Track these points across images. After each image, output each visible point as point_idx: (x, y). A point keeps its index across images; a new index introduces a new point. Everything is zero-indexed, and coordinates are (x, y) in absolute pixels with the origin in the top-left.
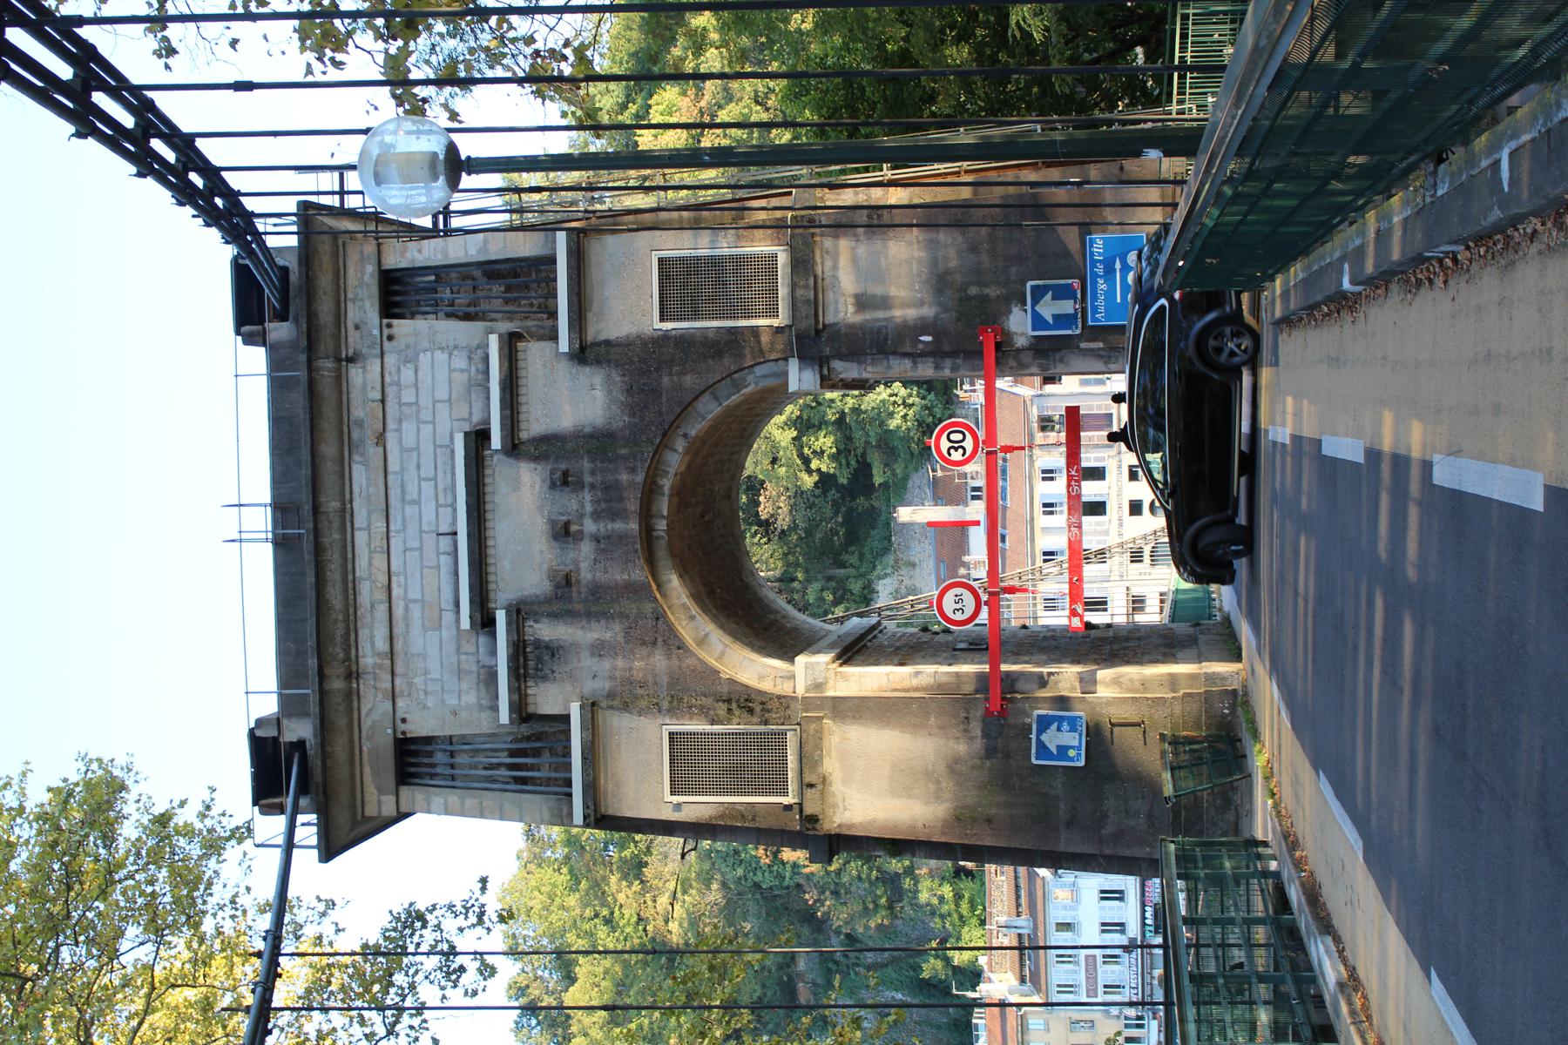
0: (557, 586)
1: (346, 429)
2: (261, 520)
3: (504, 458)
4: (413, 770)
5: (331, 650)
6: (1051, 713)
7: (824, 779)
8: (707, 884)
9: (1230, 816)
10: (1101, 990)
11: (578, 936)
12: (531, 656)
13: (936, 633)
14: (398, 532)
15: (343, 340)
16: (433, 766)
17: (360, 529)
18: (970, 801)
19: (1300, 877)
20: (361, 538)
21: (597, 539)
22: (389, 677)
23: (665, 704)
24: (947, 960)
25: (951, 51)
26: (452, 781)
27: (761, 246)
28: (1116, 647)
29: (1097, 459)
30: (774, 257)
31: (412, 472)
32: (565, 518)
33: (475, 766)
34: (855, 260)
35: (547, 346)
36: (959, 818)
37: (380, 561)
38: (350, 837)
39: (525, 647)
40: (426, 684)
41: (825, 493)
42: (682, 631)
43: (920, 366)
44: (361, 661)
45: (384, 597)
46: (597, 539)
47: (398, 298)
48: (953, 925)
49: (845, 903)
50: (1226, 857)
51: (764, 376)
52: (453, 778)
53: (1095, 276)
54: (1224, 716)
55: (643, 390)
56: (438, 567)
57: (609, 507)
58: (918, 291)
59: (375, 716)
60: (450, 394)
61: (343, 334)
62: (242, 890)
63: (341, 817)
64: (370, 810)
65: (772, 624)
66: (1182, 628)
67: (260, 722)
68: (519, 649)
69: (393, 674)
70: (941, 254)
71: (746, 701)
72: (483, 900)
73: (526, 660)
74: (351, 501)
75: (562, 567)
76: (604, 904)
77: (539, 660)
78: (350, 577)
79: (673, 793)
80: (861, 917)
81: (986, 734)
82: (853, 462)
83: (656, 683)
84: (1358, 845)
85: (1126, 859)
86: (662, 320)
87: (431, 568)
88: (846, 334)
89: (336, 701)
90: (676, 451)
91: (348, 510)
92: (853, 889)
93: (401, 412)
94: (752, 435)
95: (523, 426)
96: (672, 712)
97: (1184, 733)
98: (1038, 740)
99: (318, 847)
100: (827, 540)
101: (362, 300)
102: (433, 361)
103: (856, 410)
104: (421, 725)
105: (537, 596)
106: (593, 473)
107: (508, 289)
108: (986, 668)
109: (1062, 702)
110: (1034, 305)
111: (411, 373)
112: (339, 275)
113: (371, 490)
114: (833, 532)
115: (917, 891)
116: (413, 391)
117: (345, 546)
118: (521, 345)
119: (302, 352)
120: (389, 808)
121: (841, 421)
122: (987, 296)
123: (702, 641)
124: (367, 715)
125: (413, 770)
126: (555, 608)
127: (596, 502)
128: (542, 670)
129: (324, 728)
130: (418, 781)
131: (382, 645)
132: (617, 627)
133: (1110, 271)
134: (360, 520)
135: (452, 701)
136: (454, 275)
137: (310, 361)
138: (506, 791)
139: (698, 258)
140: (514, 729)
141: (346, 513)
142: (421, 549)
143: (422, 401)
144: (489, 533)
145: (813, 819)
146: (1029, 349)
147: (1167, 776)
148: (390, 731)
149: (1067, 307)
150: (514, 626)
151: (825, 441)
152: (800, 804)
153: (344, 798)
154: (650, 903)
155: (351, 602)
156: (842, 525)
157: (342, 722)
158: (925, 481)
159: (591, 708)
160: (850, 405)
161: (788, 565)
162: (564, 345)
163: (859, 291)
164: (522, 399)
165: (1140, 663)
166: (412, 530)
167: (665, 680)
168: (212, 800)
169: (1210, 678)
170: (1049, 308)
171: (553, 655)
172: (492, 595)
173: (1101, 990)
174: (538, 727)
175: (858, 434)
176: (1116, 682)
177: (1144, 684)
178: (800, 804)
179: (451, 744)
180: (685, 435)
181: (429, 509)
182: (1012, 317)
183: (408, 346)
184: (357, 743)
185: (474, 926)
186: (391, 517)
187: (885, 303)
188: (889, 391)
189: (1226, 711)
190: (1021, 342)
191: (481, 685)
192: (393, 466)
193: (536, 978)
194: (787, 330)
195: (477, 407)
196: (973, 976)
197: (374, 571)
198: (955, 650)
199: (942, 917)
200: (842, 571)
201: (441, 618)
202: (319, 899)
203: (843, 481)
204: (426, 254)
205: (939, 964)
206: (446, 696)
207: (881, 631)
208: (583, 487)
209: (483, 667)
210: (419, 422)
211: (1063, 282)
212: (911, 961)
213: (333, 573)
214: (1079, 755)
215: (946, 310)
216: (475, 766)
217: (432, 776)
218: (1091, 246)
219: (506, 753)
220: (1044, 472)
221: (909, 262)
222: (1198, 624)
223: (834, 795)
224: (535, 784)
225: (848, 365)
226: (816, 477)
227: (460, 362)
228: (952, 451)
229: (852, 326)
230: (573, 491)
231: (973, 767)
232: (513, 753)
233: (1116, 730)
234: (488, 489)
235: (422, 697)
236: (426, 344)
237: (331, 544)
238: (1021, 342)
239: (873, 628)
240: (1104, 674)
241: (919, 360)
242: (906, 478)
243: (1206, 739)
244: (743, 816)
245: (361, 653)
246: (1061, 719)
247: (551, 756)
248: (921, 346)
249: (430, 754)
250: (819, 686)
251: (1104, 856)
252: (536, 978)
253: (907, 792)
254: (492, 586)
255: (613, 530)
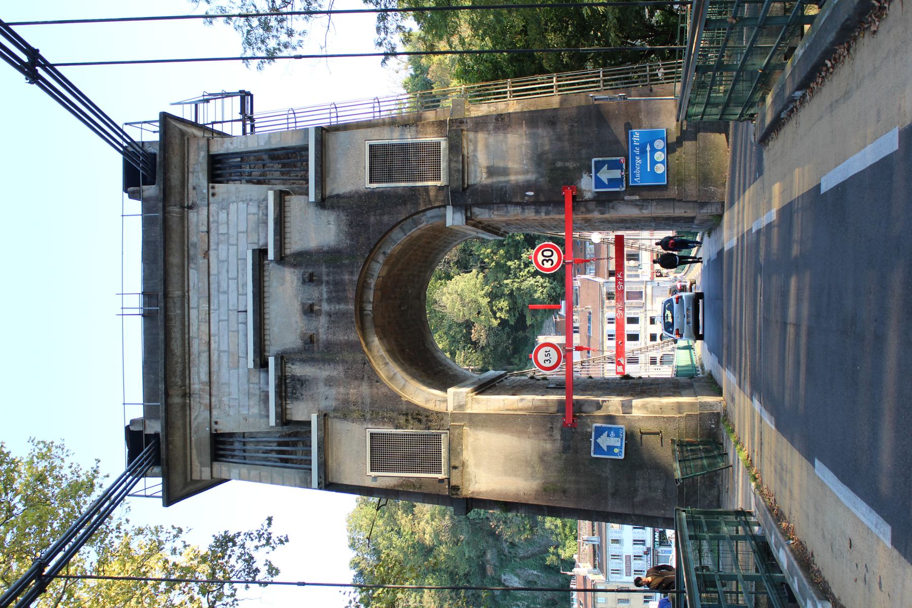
0: (305, 343)
1: (186, 248)
2: (136, 302)
3: (276, 265)
4: (222, 452)
5: (173, 379)
6: (604, 425)
7: (463, 464)
8: (444, 516)
9: (715, 492)
10: (633, 572)
11: (384, 539)
12: (289, 385)
13: (539, 380)
14: (215, 310)
15: (186, 196)
16: (233, 450)
17: (193, 308)
18: (552, 479)
19: (788, 544)
20: (193, 313)
21: (329, 315)
22: (208, 397)
23: (368, 416)
24: (558, 556)
25: (551, 36)
26: (244, 460)
27: (430, 138)
28: (645, 388)
29: (635, 313)
30: (439, 144)
31: (224, 273)
32: (310, 302)
33: (257, 451)
34: (487, 146)
35: (302, 198)
36: (546, 490)
37: (204, 327)
38: (184, 492)
39: (286, 380)
40: (229, 401)
41: (503, 329)
42: (380, 372)
43: (526, 211)
44: (192, 387)
45: (206, 348)
46: (329, 315)
47: (219, 172)
48: (562, 539)
49: (510, 527)
50: (723, 524)
51: (431, 217)
52: (245, 458)
53: (634, 155)
54: (711, 429)
55: (358, 225)
56: (238, 331)
57: (337, 296)
58: (525, 164)
59: (199, 420)
60: (247, 228)
61: (186, 192)
62: (124, 521)
63: (177, 479)
64: (196, 476)
65: (440, 372)
66: (683, 380)
67: (133, 422)
68: (282, 381)
69: (210, 395)
70: (540, 141)
71: (419, 415)
72: (270, 530)
73: (286, 388)
74: (188, 291)
75: (309, 332)
76: (396, 524)
77: (294, 388)
78: (187, 336)
79: (372, 470)
80: (518, 534)
81: (563, 438)
82: (517, 314)
83: (363, 403)
84: (884, 532)
85: (648, 517)
86: (371, 182)
87: (233, 332)
88: (481, 191)
89: (176, 412)
90: (378, 262)
91: (186, 297)
92: (514, 521)
93: (218, 239)
94: (432, 262)
95: (287, 246)
96: (372, 420)
97: (687, 439)
98: (595, 442)
99: (162, 497)
100: (504, 351)
101: (198, 172)
102: (237, 208)
103: (519, 289)
104: (226, 426)
105: (294, 349)
106: (328, 275)
107: (284, 166)
108: (564, 397)
109: (610, 419)
110: (596, 173)
111: (225, 215)
112: (184, 158)
113: (200, 285)
114: (507, 348)
115: (544, 522)
116: (226, 226)
117: (184, 318)
118: (287, 198)
119: (160, 201)
120: (206, 475)
121: (511, 294)
122: (567, 168)
123: (392, 378)
124: (195, 419)
125: (222, 452)
126: (304, 356)
127: (329, 292)
128: (295, 393)
129: (168, 425)
130: (224, 459)
131: (204, 377)
132: (341, 368)
133: (643, 152)
134: (193, 303)
135: (244, 412)
136: (252, 158)
137: (164, 207)
138: (276, 466)
139: (393, 145)
140: (280, 429)
141: (185, 298)
142: (228, 320)
143: (231, 232)
144: (266, 311)
145: (456, 488)
146: (593, 200)
147: (676, 465)
148: (208, 429)
149: (617, 174)
150: (279, 366)
151: (504, 304)
152: (449, 479)
153: (179, 468)
154: (416, 525)
155: (187, 351)
156: (511, 344)
157: (179, 423)
158: (551, 324)
159: (324, 417)
160: (516, 286)
161: (485, 363)
162: (312, 197)
163: (490, 164)
164: (287, 230)
165: (659, 396)
166: (223, 309)
167: (368, 401)
168: (98, 467)
169: (703, 405)
170: (605, 175)
171: (302, 385)
172: (267, 348)
173: (633, 572)
174: (294, 429)
175: (520, 301)
176: (644, 407)
177: (662, 408)
178: (449, 479)
179: (244, 437)
180: (384, 253)
181: (233, 296)
182: (582, 180)
183: (223, 200)
184: (188, 436)
185: (264, 545)
186: (211, 301)
187: (505, 172)
188: (535, 280)
189: (713, 426)
190: (588, 196)
191: (261, 402)
192: (213, 271)
193: (363, 559)
194: (445, 188)
195: (262, 236)
196: (571, 564)
197: (201, 333)
198: (547, 388)
199: (557, 535)
200: (511, 367)
201: (239, 362)
202: (173, 528)
203: (512, 323)
204: (235, 145)
205: (554, 558)
206: (241, 409)
207: (506, 378)
208: (322, 283)
209: (263, 391)
210: (229, 244)
211: (614, 158)
212: (541, 556)
213: (176, 334)
214: (621, 452)
215: (542, 176)
216: (257, 451)
217: (233, 456)
218: (632, 137)
219: (276, 444)
220: (609, 319)
221: (520, 147)
222: (693, 377)
223: (469, 474)
224: (293, 463)
225: (482, 210)
226: (499, 321)
227: (253, 209)
228: (545, 262)
229: (486, 186)
230: (316, 286)
231: (555, 458)
232: (280, 444)
233: (644, 436)
234: (266, 284)
235: (227, 409)
236: (234, 198)
237: (175, 316)
238: (588, 196)
239: (501, 376)
240: (637, 402)
241: (526, 207)
242: (542, 322)
243: (701, 443)
244: (414, 485)
245: (192, 382)
246: (610, 429)
247: (303, 446)
248: (526, 198)
249: (232, 443)
250: (461, 407)
251: (635, 515)
252: (363, 559)
253: (514, 473)
254: (267, 343)
255: (339, 309)
